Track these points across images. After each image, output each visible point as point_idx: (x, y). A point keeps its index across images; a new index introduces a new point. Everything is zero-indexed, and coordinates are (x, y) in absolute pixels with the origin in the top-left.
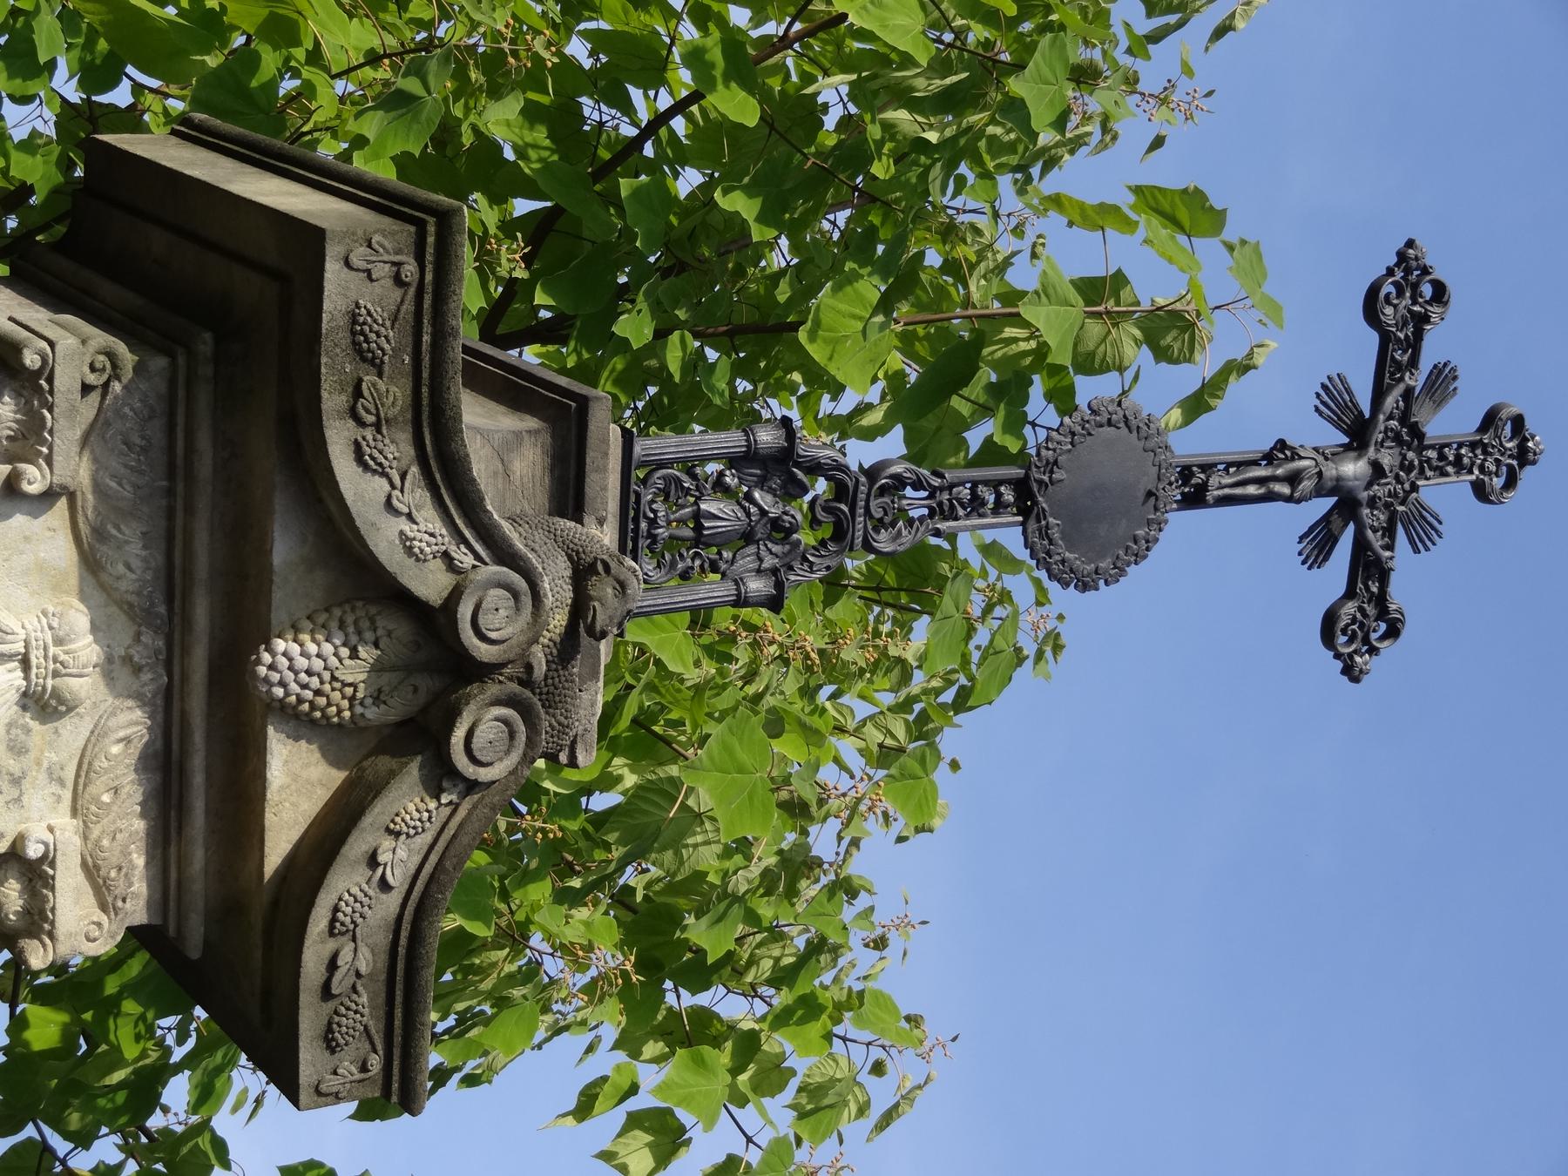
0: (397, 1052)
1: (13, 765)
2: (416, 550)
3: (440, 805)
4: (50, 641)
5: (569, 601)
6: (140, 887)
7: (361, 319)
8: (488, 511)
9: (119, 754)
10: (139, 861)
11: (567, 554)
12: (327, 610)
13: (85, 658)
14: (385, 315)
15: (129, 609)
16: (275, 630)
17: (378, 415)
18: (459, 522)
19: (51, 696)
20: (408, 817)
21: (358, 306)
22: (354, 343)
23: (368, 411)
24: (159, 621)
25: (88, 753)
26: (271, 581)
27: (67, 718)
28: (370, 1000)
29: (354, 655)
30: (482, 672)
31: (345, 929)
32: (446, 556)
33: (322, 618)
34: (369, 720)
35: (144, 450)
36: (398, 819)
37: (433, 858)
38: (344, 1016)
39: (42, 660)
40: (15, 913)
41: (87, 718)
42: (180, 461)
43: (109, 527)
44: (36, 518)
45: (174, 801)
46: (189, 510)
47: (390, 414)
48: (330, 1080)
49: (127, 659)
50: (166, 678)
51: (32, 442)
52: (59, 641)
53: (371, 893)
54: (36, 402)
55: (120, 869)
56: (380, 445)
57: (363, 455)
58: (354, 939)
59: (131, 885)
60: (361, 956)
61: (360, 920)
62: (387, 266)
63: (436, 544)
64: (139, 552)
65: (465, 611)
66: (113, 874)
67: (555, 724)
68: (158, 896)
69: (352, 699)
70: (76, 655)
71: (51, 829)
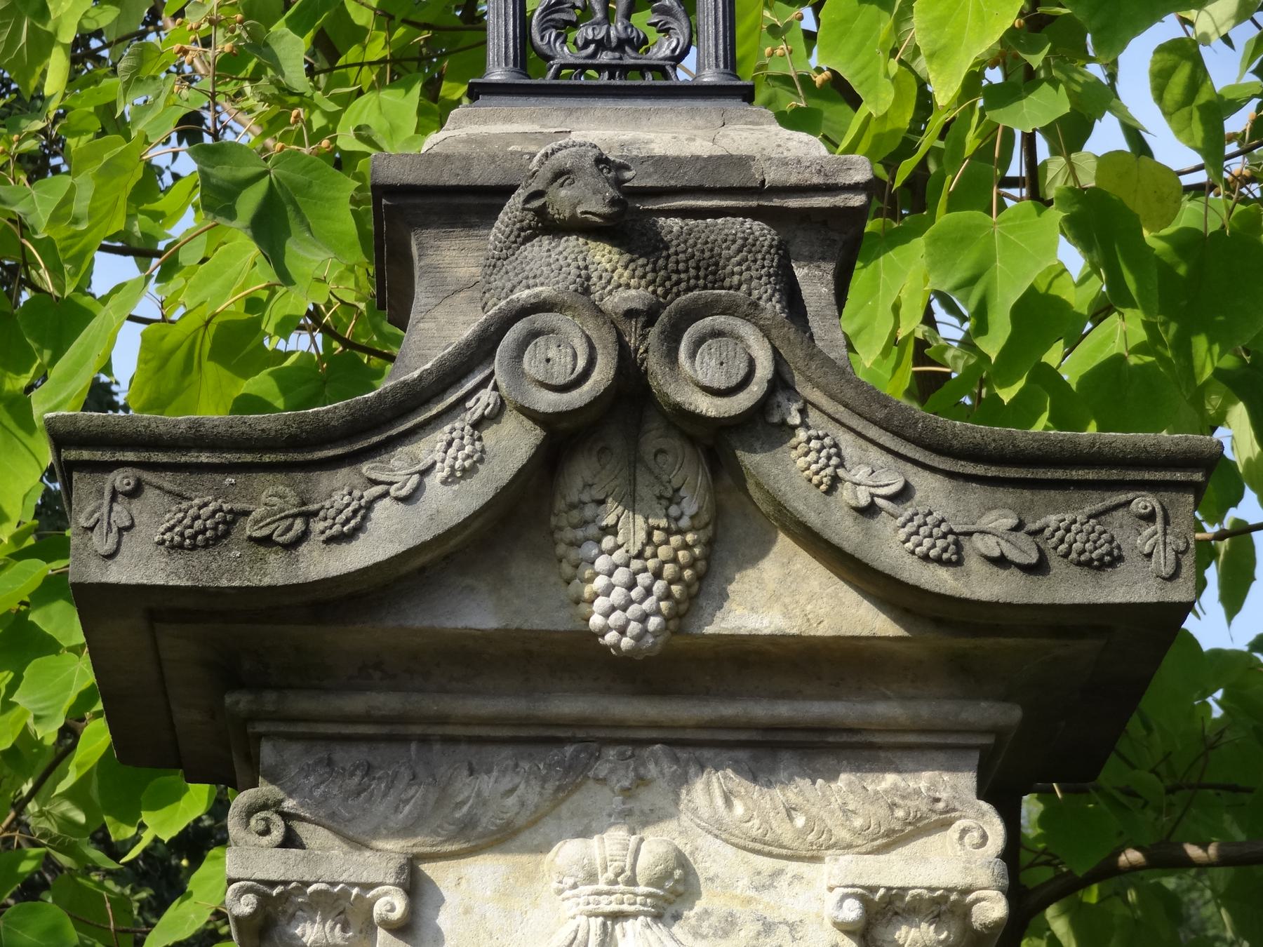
0: (1132, 475)
1: (748, 931)
2: (467, 464)
3: (804, 425)
5: (581, 240)
6: (923, 781)
7: (177, 539)
8: (420, 377)
9: (745, 804)
10: (890, 779)
11: (523, 243)
13: (614, 847)
14: (174, 508)
15: (564, 791)
16: (577, 625)
17: (295, 516)
19: (660, 887)
20: (814, 467)
21: (162, 542)
22: (206, 546)
23: (289, 529)
24: (582, 755)
25: (742, 842)
26: (518, 630)
27: (695, 866)
28: (1056, 510)
31: (952, 547)
32: (477, 425)
33: (567, 569)
34: (700, 508)
35: (369, 770)
36: (816, 479)
37: (873, 432)
38: (1071, 546)
39: (613, 898)
40: (937, 931)
41: (700, 842)
42: (385, 730)
43: (458, 815)
44: (443, 900)
45: (815, 738)
46: (443, 720)
47: (292, 498)
48: (1158, 563)
49: (627, 793)
50: (658, 746)
51: (347, 904)
52: (591, 877)
53: (910, 512)
54: (300, 900)
56: (332, 512)
57: (342, 533)
59: (918, 792)
60: (992, 525)
61: (944, 528)
62: (116, 507)
63: (462, 438)
64: (492, 780)
65: (547, 402)
66: (900, 813)
67: (738, 258)
68: (941, 757)
69: (669, 532)
70: (609, 858)
71: (831, 889)
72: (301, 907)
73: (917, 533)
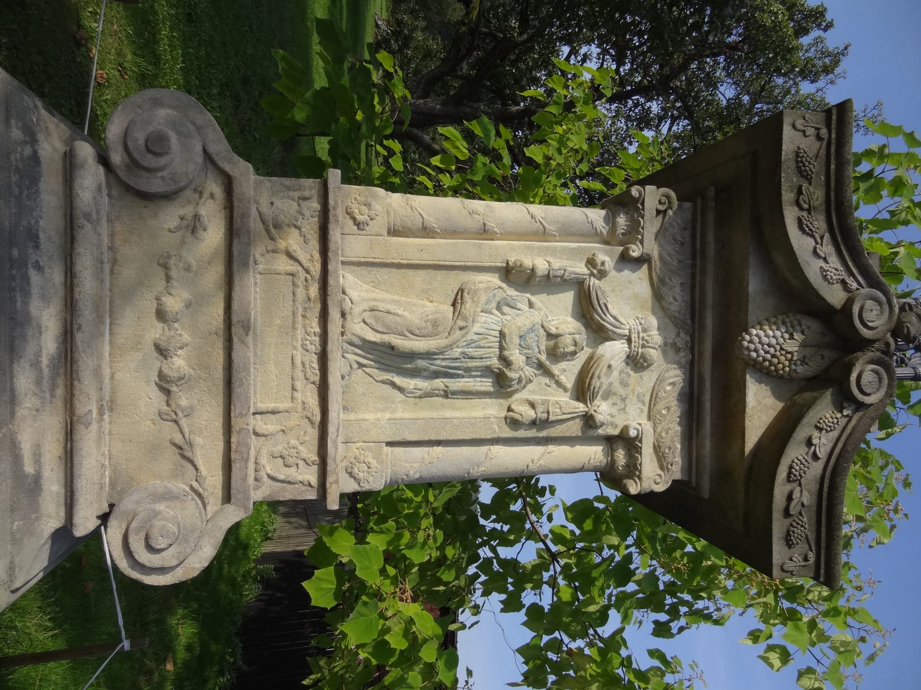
0: (823, 552)
2: (829, 277)
3: (843, 416)
4: (640, 330)
12: (775, 317)
16: (750, 324)
17: (809, 205)
18: (850, 264)
20: (826, 421)
21: (799, 148)
22: (798, 167)
23: (805, 202)
25: (656, 389)
28: (808, 521)
29: (792, 337)
30: (865, 344)
32: (843, 282)
33: (774, 320)
34: (798, 373)
36: (821, 421)
37: (840, 445)
45: (695, 417)
46: (703, 272)
49: (674, 345)
52: (645, 330)
55: (670, 448)
56: (811, 220)
58: (800, 485)
61: (803, 475)
62: (813, 129)
65: (856, 309)
66: (667, 451)
72: (632, 216)
73: (801, 463)
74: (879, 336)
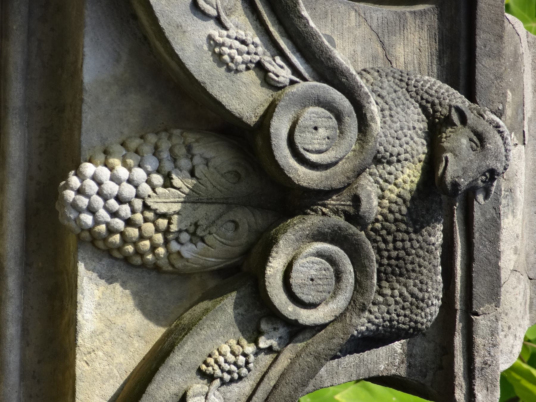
2: (226, 58)
5: (423, 157)
11: (421, 106)
16: (86, 154)
20: (221, 359)
29: (168, 183)
32: (260, 66)
33: (134, 143)
34: (187, 260)
36: (211, 361)
63: (248, 53)
67: (406, 294)
69: (166, 232)
74: (335, 184)
